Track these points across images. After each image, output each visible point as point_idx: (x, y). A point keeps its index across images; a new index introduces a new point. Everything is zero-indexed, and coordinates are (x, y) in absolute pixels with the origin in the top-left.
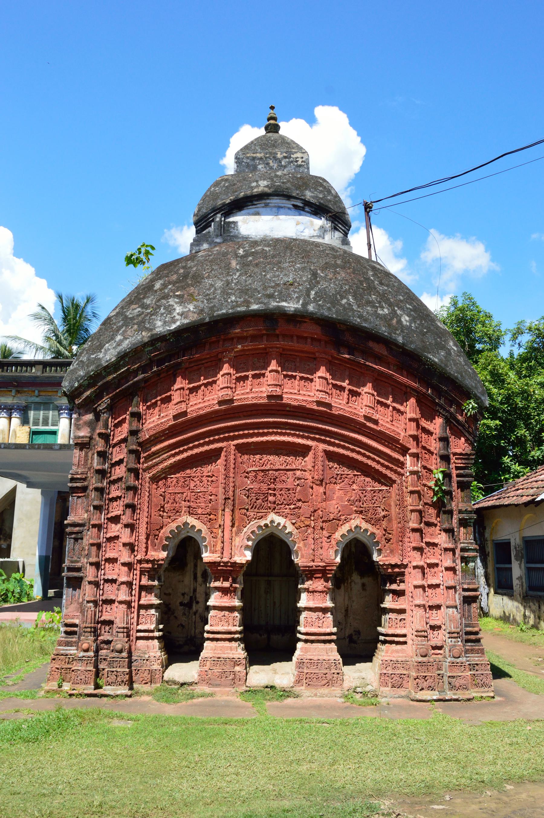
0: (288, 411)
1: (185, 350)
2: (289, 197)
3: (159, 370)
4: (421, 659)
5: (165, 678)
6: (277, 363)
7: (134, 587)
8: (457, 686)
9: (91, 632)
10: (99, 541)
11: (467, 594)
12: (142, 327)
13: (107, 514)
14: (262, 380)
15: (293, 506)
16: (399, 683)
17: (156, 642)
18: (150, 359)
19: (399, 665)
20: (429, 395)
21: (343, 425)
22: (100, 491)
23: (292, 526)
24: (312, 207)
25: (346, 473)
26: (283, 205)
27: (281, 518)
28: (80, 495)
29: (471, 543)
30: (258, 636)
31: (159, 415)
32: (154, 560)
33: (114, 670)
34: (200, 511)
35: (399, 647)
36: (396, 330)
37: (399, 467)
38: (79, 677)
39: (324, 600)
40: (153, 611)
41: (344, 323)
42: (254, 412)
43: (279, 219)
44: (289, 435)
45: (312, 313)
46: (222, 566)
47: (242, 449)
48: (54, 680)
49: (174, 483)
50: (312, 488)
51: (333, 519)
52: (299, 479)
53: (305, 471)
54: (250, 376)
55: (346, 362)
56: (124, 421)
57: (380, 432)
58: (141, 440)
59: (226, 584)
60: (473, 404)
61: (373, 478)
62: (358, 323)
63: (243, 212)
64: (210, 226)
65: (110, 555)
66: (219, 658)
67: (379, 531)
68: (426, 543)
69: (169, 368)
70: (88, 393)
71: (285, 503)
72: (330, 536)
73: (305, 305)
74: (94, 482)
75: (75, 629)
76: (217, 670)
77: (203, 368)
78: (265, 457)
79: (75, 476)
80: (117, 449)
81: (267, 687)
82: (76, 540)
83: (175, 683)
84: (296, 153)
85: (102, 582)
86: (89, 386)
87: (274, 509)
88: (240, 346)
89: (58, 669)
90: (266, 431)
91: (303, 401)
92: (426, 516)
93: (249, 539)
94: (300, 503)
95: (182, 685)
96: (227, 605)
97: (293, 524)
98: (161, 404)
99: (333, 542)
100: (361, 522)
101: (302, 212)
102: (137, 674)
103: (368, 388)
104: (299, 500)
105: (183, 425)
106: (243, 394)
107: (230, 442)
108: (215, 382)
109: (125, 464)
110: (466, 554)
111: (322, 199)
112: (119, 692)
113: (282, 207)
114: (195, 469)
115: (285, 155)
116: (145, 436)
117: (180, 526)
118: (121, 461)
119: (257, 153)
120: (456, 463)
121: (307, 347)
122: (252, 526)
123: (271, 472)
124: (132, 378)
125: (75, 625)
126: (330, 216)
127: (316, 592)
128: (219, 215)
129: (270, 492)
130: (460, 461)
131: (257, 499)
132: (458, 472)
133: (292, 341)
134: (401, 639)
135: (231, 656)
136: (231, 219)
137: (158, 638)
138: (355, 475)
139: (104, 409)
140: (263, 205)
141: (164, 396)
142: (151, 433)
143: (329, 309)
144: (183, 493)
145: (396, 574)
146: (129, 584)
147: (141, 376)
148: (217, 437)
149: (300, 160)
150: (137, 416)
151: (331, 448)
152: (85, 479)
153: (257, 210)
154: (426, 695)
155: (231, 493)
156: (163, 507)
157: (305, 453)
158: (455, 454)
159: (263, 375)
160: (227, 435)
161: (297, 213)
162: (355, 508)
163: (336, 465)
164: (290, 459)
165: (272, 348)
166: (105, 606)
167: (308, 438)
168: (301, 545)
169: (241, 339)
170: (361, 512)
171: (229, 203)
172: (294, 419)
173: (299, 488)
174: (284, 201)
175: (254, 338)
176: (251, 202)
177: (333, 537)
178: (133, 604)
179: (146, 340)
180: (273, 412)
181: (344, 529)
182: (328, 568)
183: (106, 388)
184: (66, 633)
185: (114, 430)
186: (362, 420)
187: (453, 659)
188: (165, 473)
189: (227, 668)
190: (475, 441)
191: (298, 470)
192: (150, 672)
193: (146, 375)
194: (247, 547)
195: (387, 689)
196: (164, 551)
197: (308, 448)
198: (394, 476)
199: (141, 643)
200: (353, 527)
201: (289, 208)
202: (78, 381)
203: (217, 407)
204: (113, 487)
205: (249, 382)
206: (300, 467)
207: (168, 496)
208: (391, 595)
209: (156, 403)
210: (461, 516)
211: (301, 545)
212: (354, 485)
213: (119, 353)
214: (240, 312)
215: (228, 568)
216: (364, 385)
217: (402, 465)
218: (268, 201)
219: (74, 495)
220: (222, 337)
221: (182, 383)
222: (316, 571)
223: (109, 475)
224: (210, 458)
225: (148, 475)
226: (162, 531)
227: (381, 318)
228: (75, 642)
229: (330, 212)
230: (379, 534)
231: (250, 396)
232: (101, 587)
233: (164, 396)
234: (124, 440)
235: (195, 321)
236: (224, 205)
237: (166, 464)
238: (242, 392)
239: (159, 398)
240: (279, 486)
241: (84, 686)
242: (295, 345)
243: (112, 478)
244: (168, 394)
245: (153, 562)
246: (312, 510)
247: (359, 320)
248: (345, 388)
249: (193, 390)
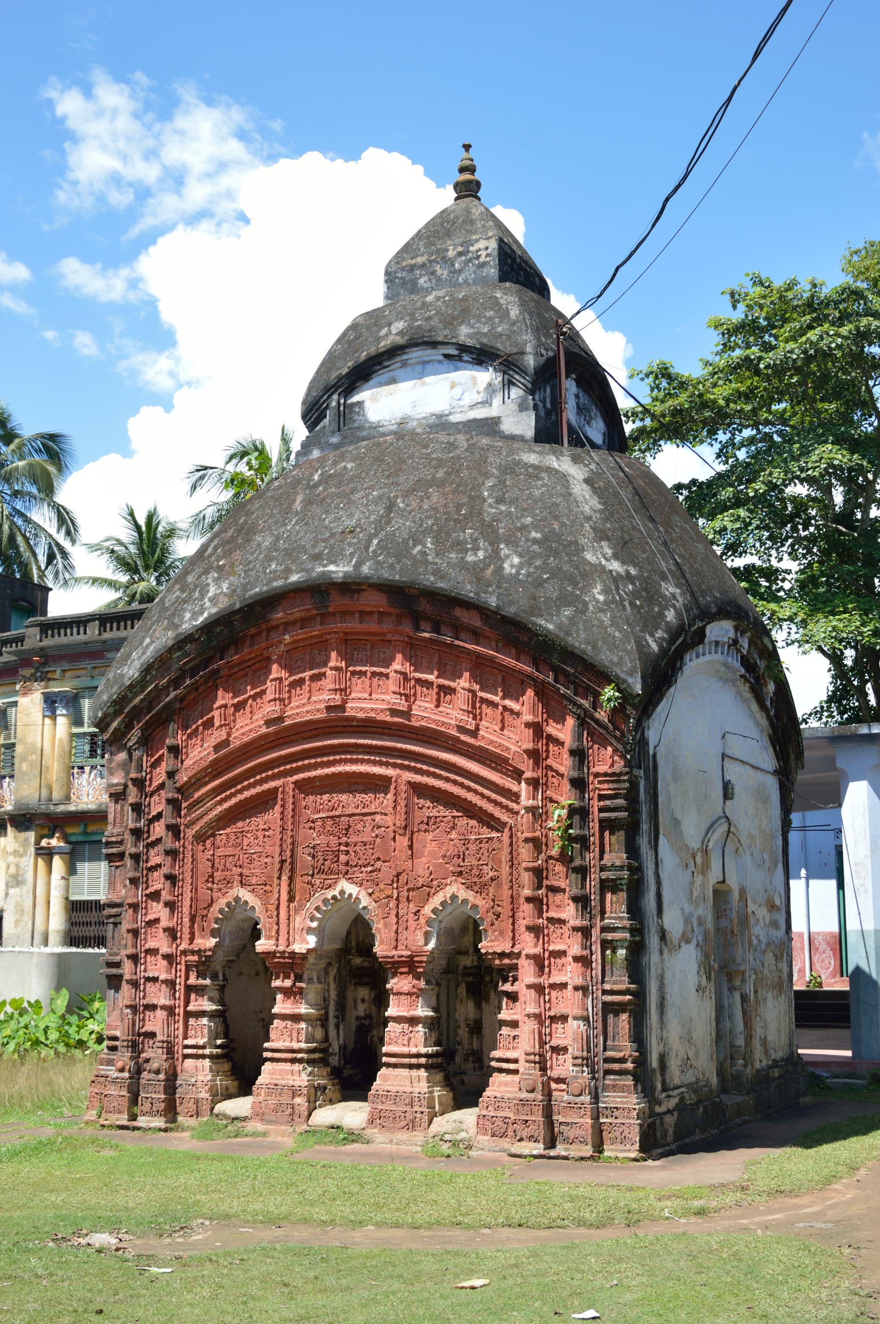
1: (222, 652)
3: (193, 684)
4: (524, 1095)
5: (216, 1111)
6: (339, 654)
7: (178, 987)
8: (572, 1137)
9: (128, 1047)
10: (135, 926)
11: (609, 998)
13: (147, 888)
15: (370, 869)
16: (503, 1131)
17: (207, 1063)
18: (180, 669)
19: (504, 1105)
20: (549, 683)
22: (136, 857)
23: (367, 898)
24: (471, 353)
25: (442, 814)
26: (428, 359)
27: (353, 886)
29: (621, 918)
32: (200, 950)
35: (509, 1078)
36: (490, 585)
37: (512, 801)
39: (411, 1006)
40: (205, 1021)
41: (411, 586)
42: (314, 732)
43: (424, 384)
44: (362, 761)
45: (367, 577)
47: (306, 787)
48: (93, 1107)
51: (423, 885)
53: (386, 815)
57: (480, 748)
58: (178, 785)
59: (288, 983)
60: (609, 692)
61: (481, 821)
62: (432, 583)
63: (372, 382)
65: (151, 944)
67: (484, 902)
68: (548, 919)
70: (115, 724)
71: (360, 863)
72: (419, 911)
73: (357, 566)
74: (130, 848)
76: (272, 1101)
80: (155, 798)
81: (333, 1127)
82: (116, 924)
83: (225, 1116)
84: (477, 241)
85: (142, 981)
86: (117, 714)
87: (347, 873)
88: (287, 637)
90: (331, 758)
91: (372, 709)
92: (550, 876)
93: (312, 919)
94: (378, 864)
96: (288, 1012)
97: (370, 895)
98: (204, 730)
99: (422, 921)
100: (458, 889)
101: (460, 364)
102: (181, 1103)
103: (463, 683)
104: (379, 859)
106: (298, 707)
108: (264, 692)
110: (610, 936)
111: (485, 335)
113: (429, 362)
114: (248, 821)
115: (460, 249)
116: (183, 778)
118: (159, 816)
119: (417, 256)
120: (600, 790)
121: (372, 626)
122: (317, 900)
123: (343, 819)
127: (401, 994)
128: (335, 397)
129: (342, 848)
130: (606, 786)
131: (325, 860)
132: (602, 803)
134: (512, 1066)
135: (291, 1083)
136: (355, 399)
137: (211, 1057)
141: (205, 718)
142: (191, 774)
143: (391, 567)
145: (508, 973)
146: (171, 984)
147: (172, 695)
148: (270, 773)
149: (483, 253)
150: (175, 750)
151: (418, 778)
152: (121, 843)
153: (391, 374)
154: (525, 1147)
155: (288, 853)
156: (212, 876)
158: (597, 775)
159: (324, 674)
160: (282, 768)
161: (452, 367)
163: (428, 804)
164: (368, 797)
166: (147, 1013)
167: (387, 764)
168: (380, 926)
169: (287, 626)
170: (460, 874)
171: (347, 374)
172: (365, 738)
173: (378, 840)
174: (429, 352)
175: (305, 622)
177: (422, 912)
178: (177, 1011)
179: (170, 643)
180: (339, 729)
181: (436, 901)
182: (416, 959)
183: (136, 714)
184: (461, 1071)
185: (151, 772)
186: (454, 733)
187: (571, 1097)
189: (285, 1099)
190: (628, 752)
192: (197, 1102)
193: (179, 692)
194: (310, 931)
195: (486, 1138)
196: (214, 937)
197: (387, 779)
198: (504, 817)
199: (189, 1062)
200: (448, 896)
201: (440, 362)
203: (264, 730)
204: (152, 852)
205: (306, 688)
206: (378, 810)
210: (605, 875)
211: (380, 926)
212: (454, 832)
214: (277, 588)
217: (515, 797)
218: (405, 357)
220: (263, 626)
221: (223, 698)
222: (400, 964)
223: (146, 835)
224: (266, 803)
225: (190, 833)
227: (468, 569)
230: (483, 907)
232: (142, 987)
233: (205, 718)
234: (162, 786)
236: (340, 378)
240: (353, 839)
241: (117, 1116)
242: (353, 625)
243: (149, 840)
245: (199, 952)
246: (395, 873)
247: (432, 578)
248: (432, 683)
249: (239, 706)
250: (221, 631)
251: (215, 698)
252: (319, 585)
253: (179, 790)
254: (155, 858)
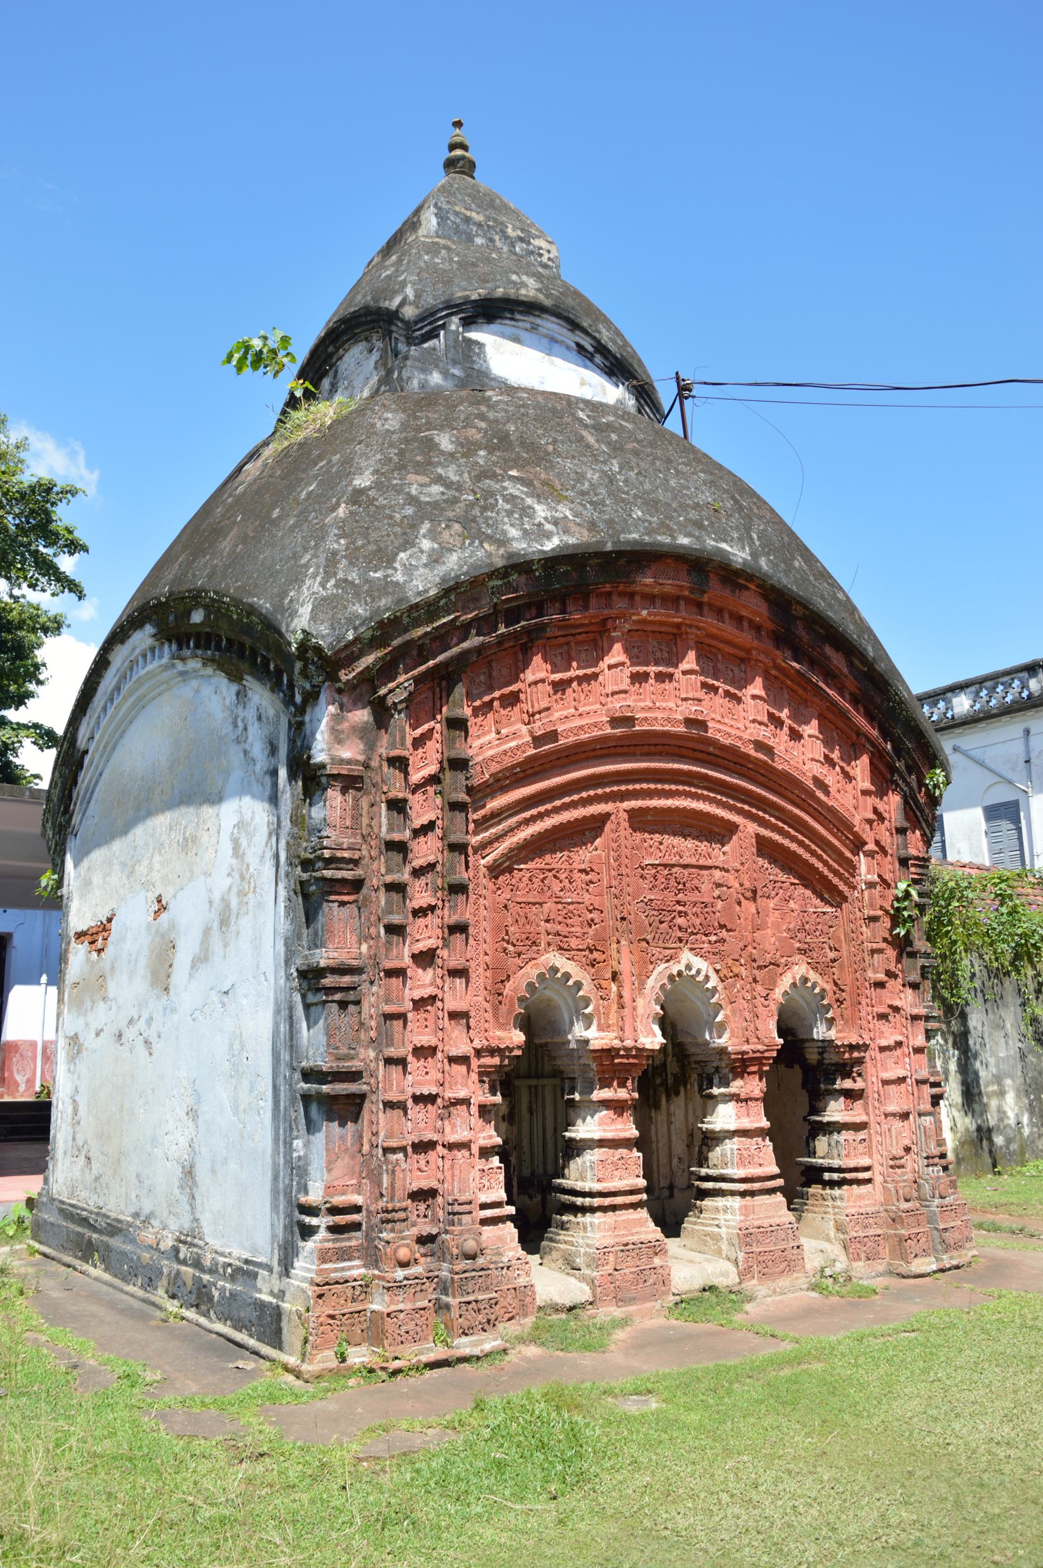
0: (710, 754)
1: (562, 600)
2: (575, 326)
12: (472, 529)
14: (667, 685)
15: (713, 938)
21: (782, 790)
24: (606, 359)
26: (560, 338)
28: (346, 898)
30: (527, 1200)
31: (498, 733)
33: (471, 1298)
34: (574, 943)
35: (864, 1189)
38: (404, 1328)
41: (804, 604)
43: (553, 363)
46: (622, 1057)
47: (639, 821)
50: (739, 903)
52: (718, 885)
53: (727, 871)
54: (652, 675)
55: (787, 676)
56: (428, 735)
57: (831, 810)
58: (475, 782)
63: (493, 327)
64: (437, 336)
66: (626, 1245)
69: (527, 631)
75: (356, 1217)
76: (628, 1270)
78: (669, 840)
79: (339, 854)
81: (704, 1290)
83: (557, 1309)
86: (375, 642)
88: (644, 613)
89: (332, 1317)
90: (673, 787)
95: (571, 1309)
105: (550, 757)
107: (618, 804)
109: (439, 832)
112: (487, 1347)
117: (544, 974)
124: (455, 640)
125: (357, 1209)
126: (634, 386)
127: (751, 1099)
128: (455, 319)
131: (661, 922)
134: (865, 1175)
136: (473, 335)
138: (792, 884)
139: (401, 702)
140: (528, 326)
144: (541, 904)
150: (457, 724)
157: (724, 836)
160: (615, 788)
162: (798, 945)
164: (704, 846)
165: (690, 626)
169: (650, 599)
171: (476, 301)
174: (565, 332)
175: (672, 601)
176: (512, 312)
183: (420, 651)
188: (509, 858)
191: (716, 868)
193: (487, 639)
195: (861, 1264)
200: (798, 977)
201: (568, 348)
202: (355, 629)
207: (514, 908)
208: (842, 1099)
209: (489, 705)
213: (444, 580)
215: (631, 1061)
216: (807, 722)
217: (852, 868)
218: (539, 321)
219: (332, 898)
220: (621, 588)
224: (582, 833)
226: (508, 985)
229: (635, 378)
234: (434, 780)
235: (588, 545)
236: (467, 301)
237: (515, 839)
239: (497, 694)
241: (415, 1348)
242: (728, 629)
244: (513, 688)
249: (560, 687)
250: (566, 572)
251: (526, 665)
252: (710, 561)
253: (470, 790)
254: (421, 895)
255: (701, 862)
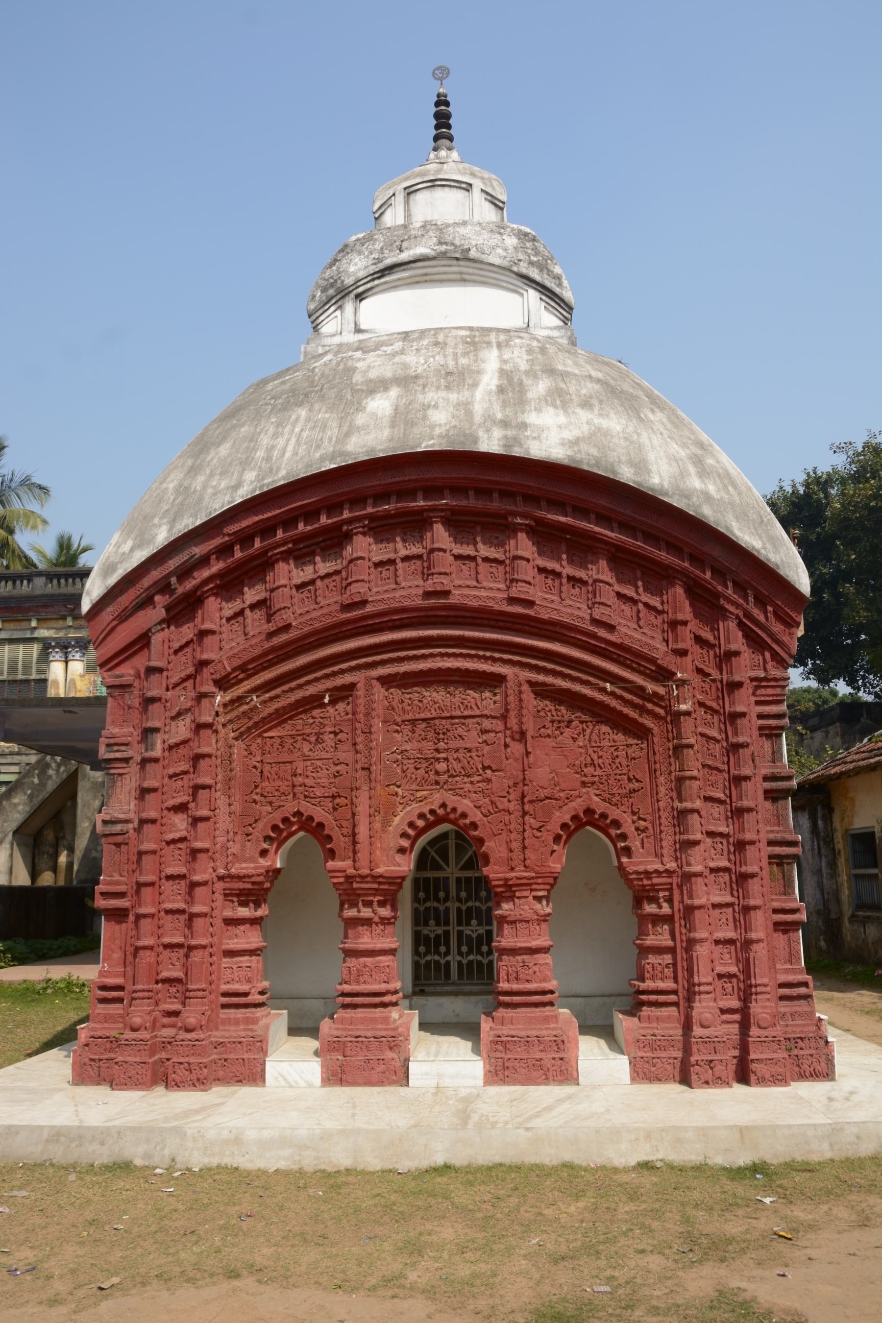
49: (276, 746)
66: (357, 1037)
77: (318, 551)
91: (489, 598)
131: (417, 769)
133: (468, 498)
203: (419, 602)
228: (121, 1016)
231: (397, 594)
238: (385, 588)
240: (453, 744)
255: (466, 713)
